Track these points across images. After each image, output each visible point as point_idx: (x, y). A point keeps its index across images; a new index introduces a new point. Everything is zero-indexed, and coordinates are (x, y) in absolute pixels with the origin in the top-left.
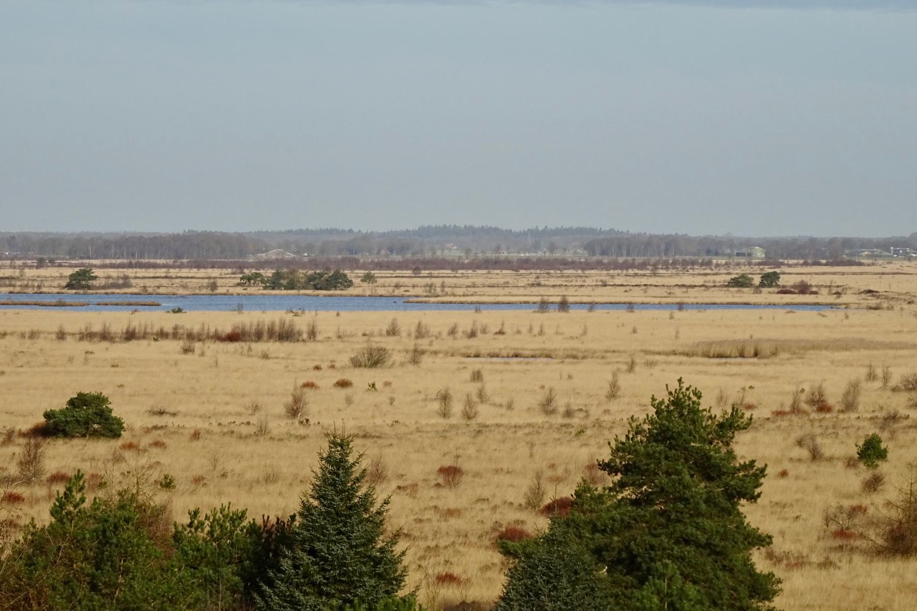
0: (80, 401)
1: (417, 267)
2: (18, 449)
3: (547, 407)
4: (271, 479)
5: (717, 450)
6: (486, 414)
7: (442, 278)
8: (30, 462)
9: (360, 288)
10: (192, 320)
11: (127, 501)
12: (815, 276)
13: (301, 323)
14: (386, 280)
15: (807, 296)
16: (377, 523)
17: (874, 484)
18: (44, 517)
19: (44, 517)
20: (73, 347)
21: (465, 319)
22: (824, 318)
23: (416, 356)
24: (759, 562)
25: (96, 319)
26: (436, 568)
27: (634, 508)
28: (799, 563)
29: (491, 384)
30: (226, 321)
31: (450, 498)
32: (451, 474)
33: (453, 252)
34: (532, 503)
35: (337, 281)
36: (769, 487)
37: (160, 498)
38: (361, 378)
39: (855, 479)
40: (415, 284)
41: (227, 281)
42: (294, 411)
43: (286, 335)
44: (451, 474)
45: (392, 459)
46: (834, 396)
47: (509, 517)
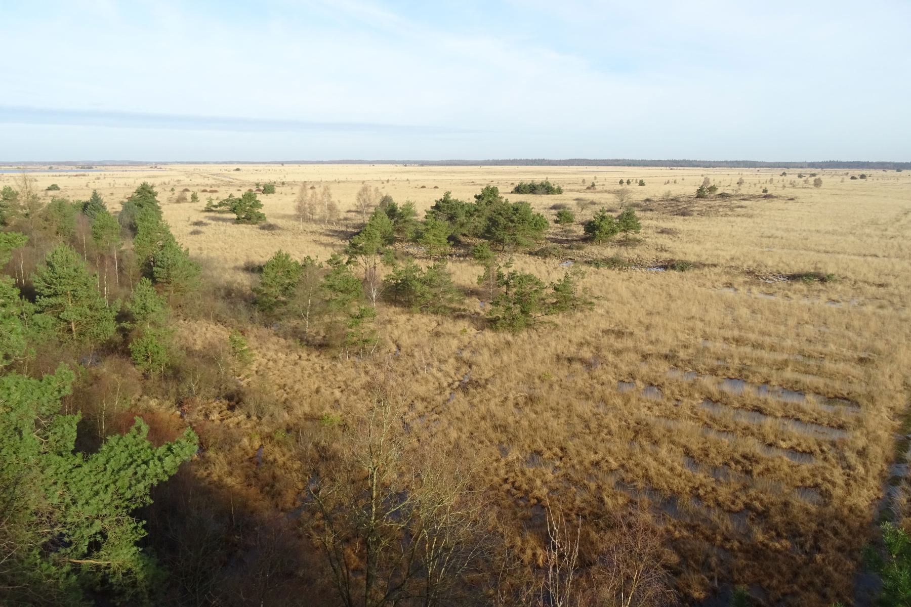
0: (53, 185)
1: (103, 166)
2: (44, 192)
3: (125, 185)
4: (84, 195)
5: (151, 190)
6: (116, 186)
7: (107, 167)
8: (46, 195)
9: (95, 169)
10: (69, 173)
11: (63, 199)
12: (162, 167)
13: (86, 173)
14: (99, 168)
15: (300, 178)
16: (102, 201)
17: (173, 194)
18: (50, 202)
19: (50, 202)
20: (51, 178)
21: (111, 173)
22: (348, 209)
23: (105, 178)
24: (158, 204)
25: (54, 174)
26: (111, 207)
27: (104, 448)
28: (164, 204)
29: (117, 181)
30: (75, 174)
31: (112, 197)
32: (112, 194)
33: (108, 164)
34: (125, 197)
35: (91, 168)
36: (158, 195)
37: (68, 198)
38: (97, 181)
39: (170, 194)
40: (103, 168)
41: (74, 168)
42: (87, 186)
43: (84, 175)
44: (112, 194)
45: (103, 192)
46: (167, 182)
47: (121, 200)
